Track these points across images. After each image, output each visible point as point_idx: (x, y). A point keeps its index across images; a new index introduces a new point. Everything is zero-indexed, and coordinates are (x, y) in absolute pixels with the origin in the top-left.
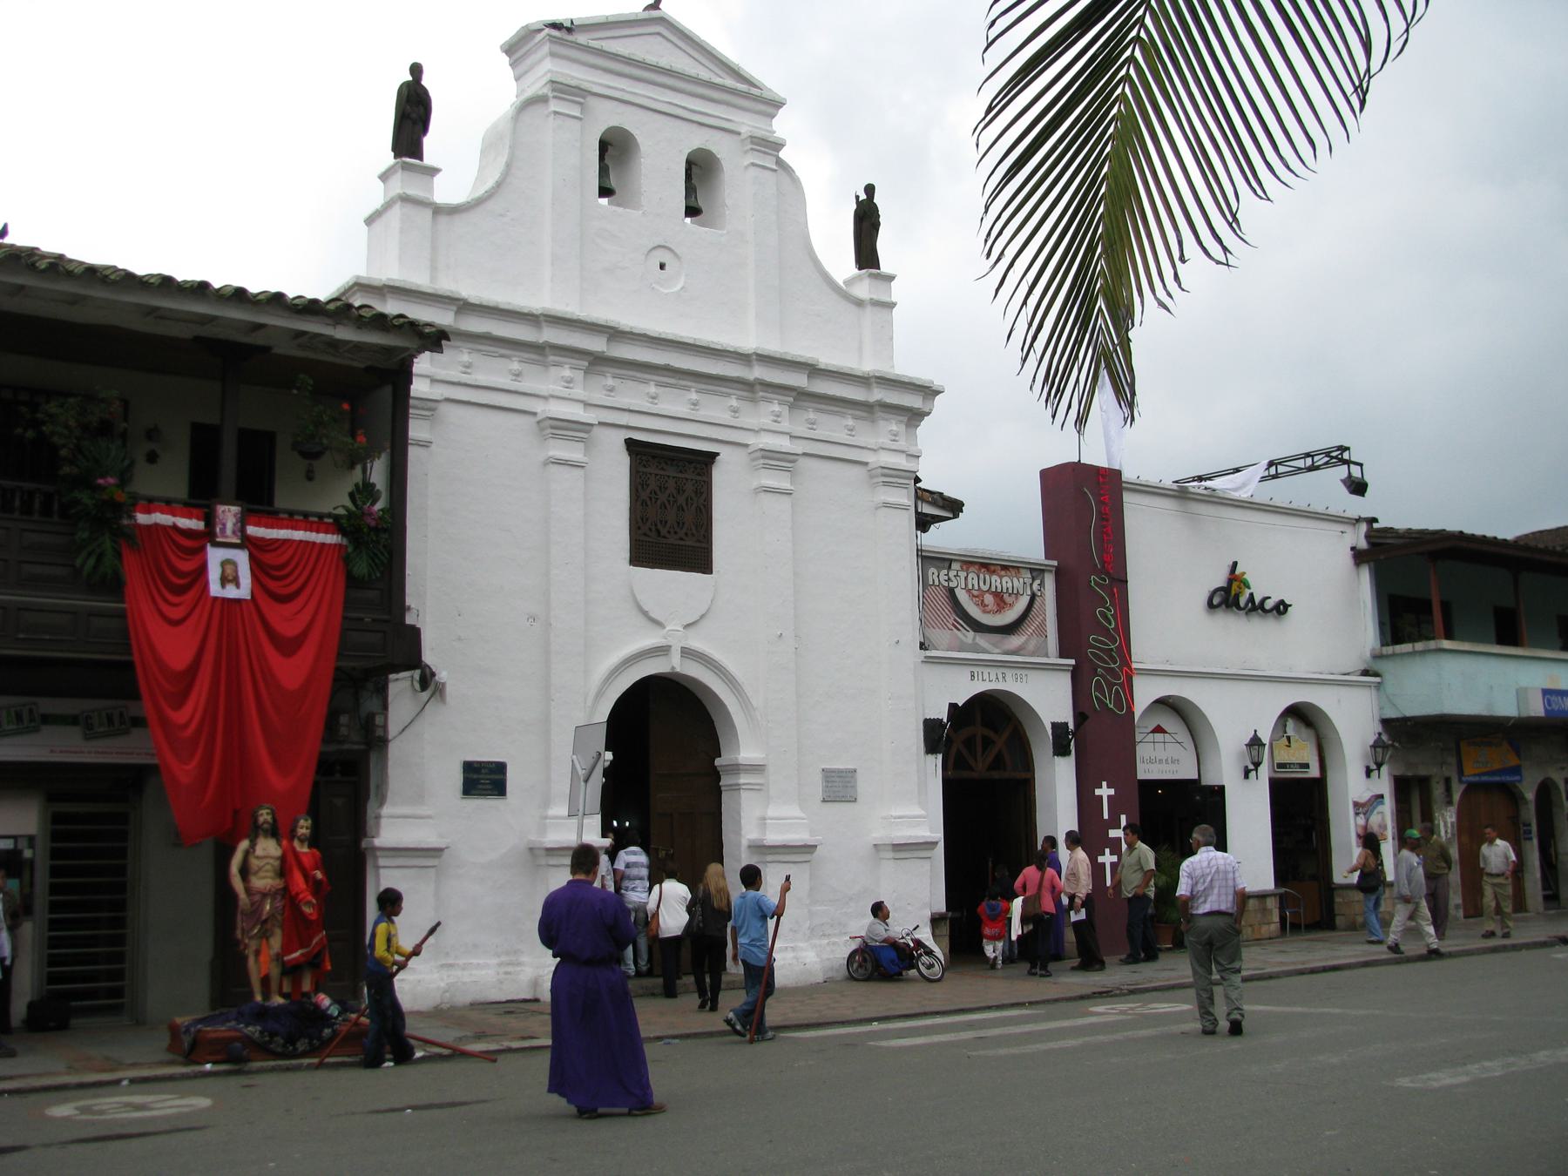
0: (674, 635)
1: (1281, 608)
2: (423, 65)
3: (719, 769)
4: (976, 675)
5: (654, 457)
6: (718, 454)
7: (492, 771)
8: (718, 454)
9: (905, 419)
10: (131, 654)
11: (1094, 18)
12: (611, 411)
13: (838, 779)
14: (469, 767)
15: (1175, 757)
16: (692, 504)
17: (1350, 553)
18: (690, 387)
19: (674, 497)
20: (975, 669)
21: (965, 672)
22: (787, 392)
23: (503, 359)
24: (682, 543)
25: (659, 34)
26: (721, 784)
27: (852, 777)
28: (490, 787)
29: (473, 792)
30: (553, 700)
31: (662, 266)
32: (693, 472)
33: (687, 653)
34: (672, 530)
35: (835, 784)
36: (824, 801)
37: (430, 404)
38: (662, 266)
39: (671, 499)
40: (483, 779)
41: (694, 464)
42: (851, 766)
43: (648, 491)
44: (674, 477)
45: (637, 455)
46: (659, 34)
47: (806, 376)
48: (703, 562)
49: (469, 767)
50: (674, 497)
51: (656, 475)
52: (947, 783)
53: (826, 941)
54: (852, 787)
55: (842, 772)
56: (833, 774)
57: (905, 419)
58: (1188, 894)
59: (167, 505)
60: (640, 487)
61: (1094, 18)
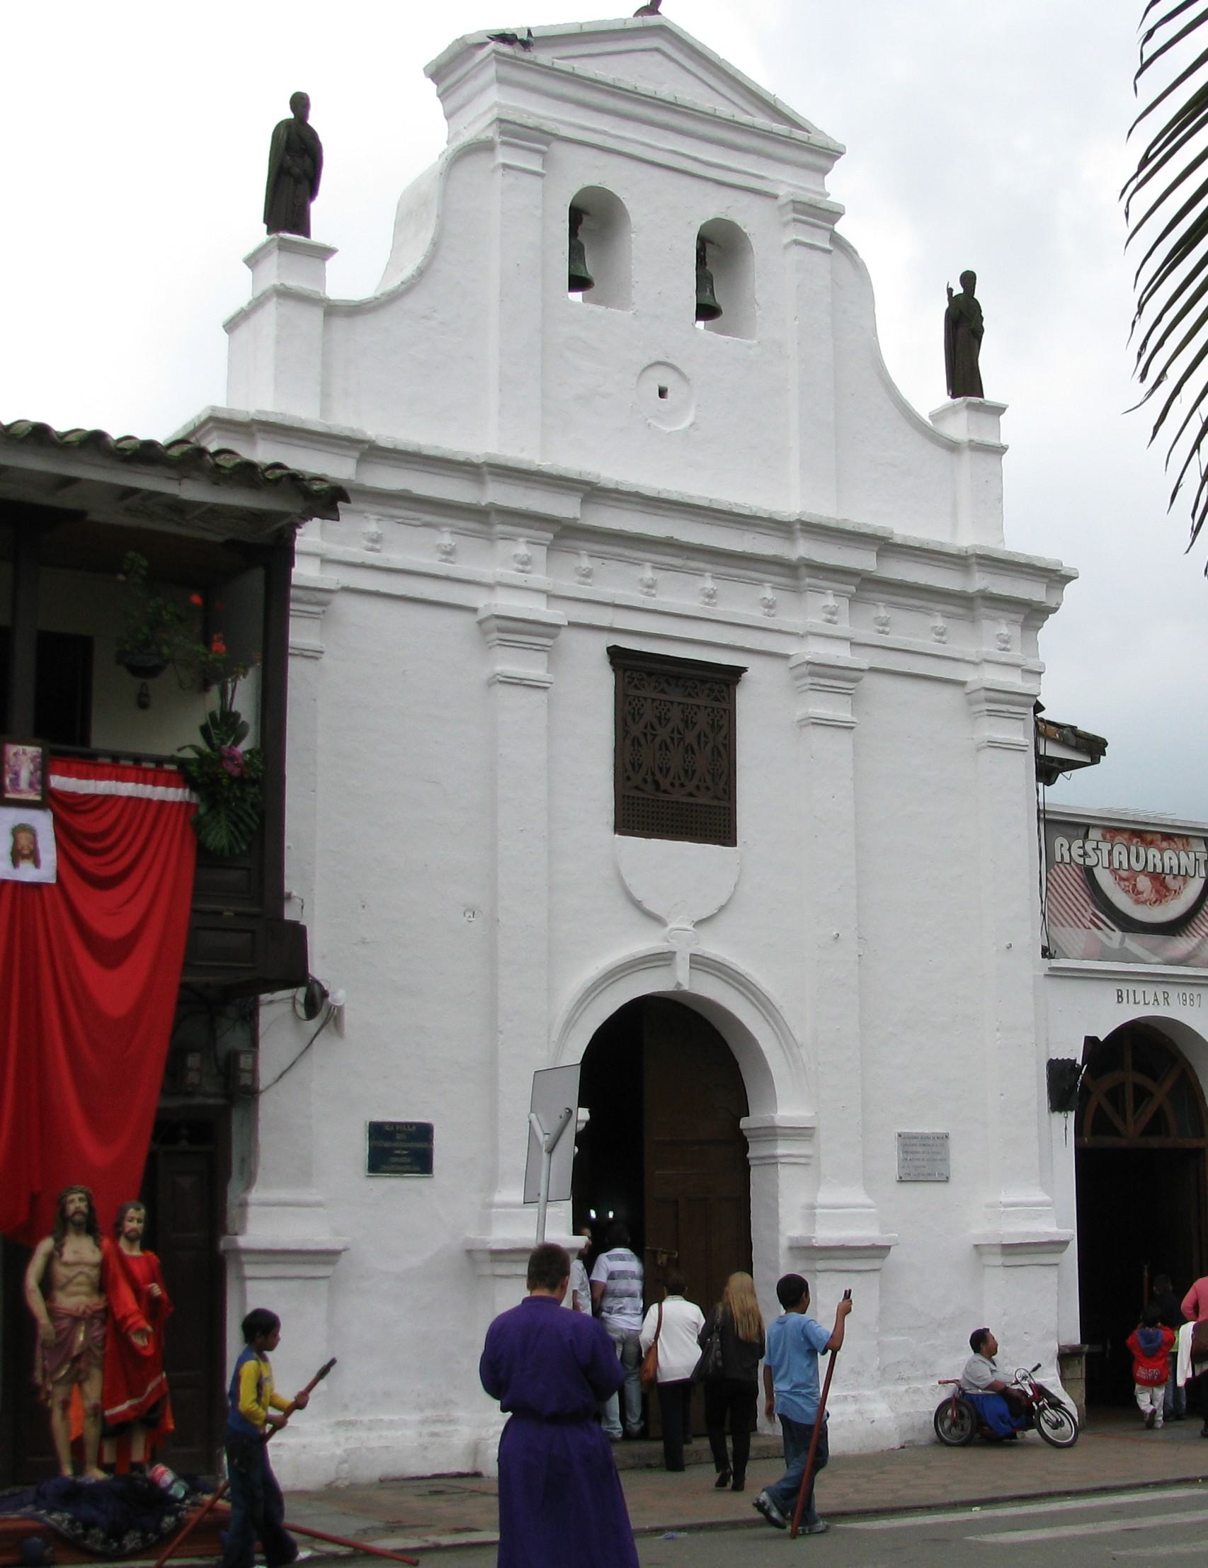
3: (745, 1133)
6: (744, 669)
8: (744, 669)
13: (920, 1149)
14: (378, 1132)
16: (706, 743)
19: (679, 733)
20: (1124, 987)
21: (1110, 990)
24: (691, 800)
25: (657, 50)
26: (748, 1155)
29: (384, 1167)
31: (662, 393)
33: (700, 963)
34: (677, 783)
35: (918, 1156)
36: (901, 1181)
37: (321, 596)
38: (662, 393)
39: (676, 735)
41: (708, 685)
42: (939, 1130)
43: (641, 725)
46: (657, 50)
49: (378, 1132)
50: (679, 733)
51: (654, 700)
54: (941, 1160)
56: (914, 1141)
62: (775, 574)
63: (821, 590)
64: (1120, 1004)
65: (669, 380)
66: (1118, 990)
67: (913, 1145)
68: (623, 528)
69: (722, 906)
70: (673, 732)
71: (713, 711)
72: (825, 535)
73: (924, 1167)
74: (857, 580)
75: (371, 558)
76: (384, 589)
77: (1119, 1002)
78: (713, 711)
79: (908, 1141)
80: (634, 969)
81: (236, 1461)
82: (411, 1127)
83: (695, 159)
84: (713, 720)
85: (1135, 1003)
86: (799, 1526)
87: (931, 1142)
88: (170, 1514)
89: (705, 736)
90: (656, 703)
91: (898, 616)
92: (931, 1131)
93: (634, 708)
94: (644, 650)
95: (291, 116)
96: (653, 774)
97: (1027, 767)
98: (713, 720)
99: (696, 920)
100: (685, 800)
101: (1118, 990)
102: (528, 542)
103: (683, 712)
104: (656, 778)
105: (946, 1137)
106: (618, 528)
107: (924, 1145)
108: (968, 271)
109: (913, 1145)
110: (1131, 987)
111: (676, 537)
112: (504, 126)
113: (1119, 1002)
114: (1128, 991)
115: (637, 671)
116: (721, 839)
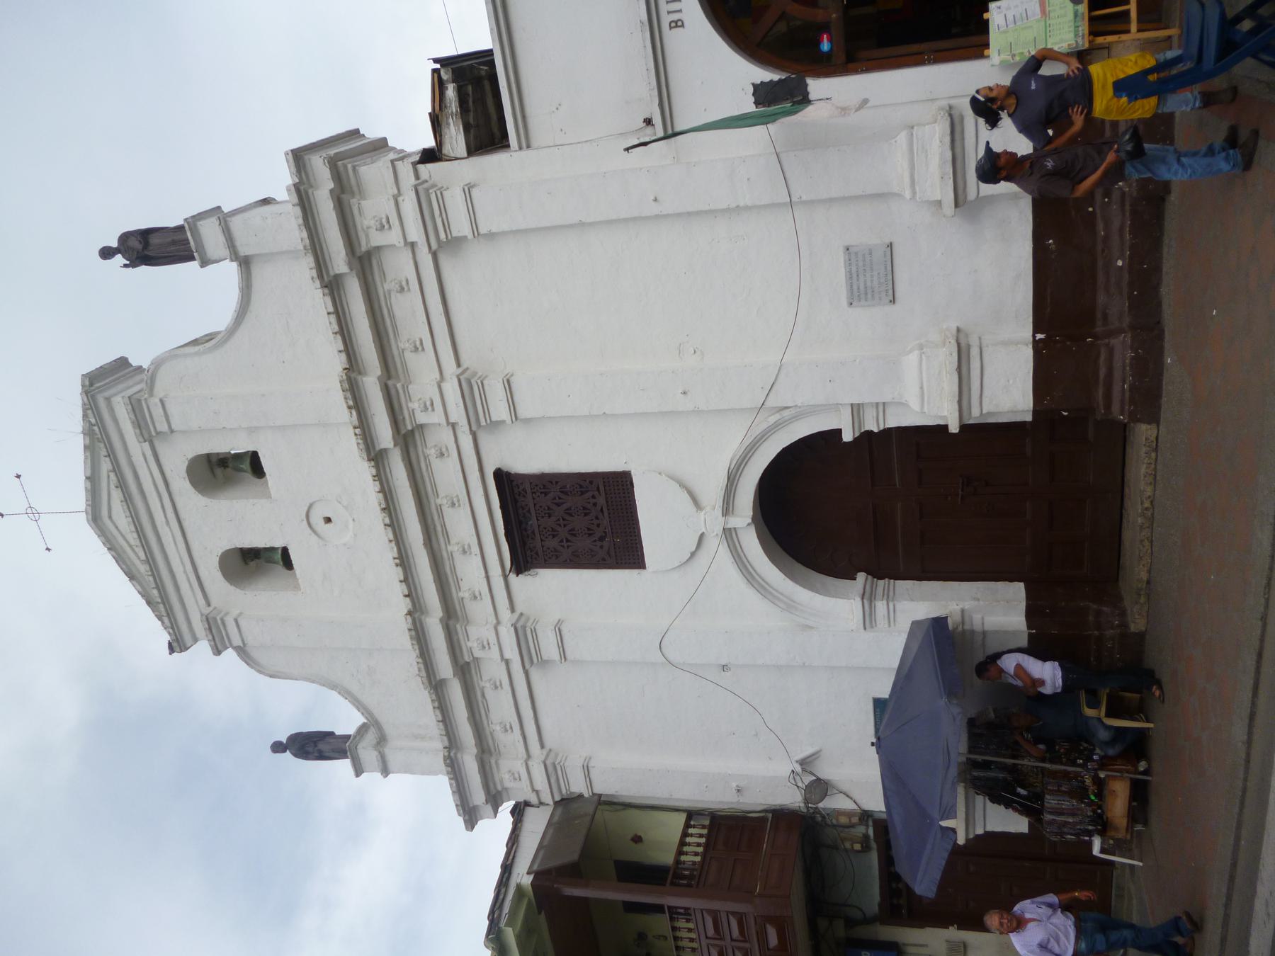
0: (713, 521)
1: (429, 59)
2: (271, 753)
3: (857, 434)
4: (675, 17)
9: (354, 201)
12: (495, 592)
13: (862, 278)
15: (799, 197)
16: (560, 498)
18: (436, 504)
20: (666, 19)
21: (673, 39)
22: (393, 392)
23: (486, 695)
24: (602, 488)
25: (110, 517)
26: (876, 430)
30: (804, 664)
31: (328, 520)
32: (524, 496)
33: (728, 506)
34: (592, 501)
35: (869, 284)
36: (893, 301)
37: (550, 769)
38: (328, 520)
41: (517, 497)
42: (841, 258)
43: (559, 529)
44: (538, 520)
45: (527, 562)
46: (110, 517)
47: (364, 379)
48: (620, 487)
51: (542, 540)
54: (871, 254)
55: (850, 272)
56: (855, 287)
57: (384, 506)
58: (1087, 45)
59: (692, 951)
62: (439, 544)
63: (411, 414)
64: (686, 24)
66: (671, 28)
67: (859, 289)
68: (432, 581)
69: (680, 486)
71: (535, 493)
72: (432, 664)
73: (879, 274)
74: (451, 623)
75: (476, 549)
76: (536, 738)
77: (683, 26)
78: (535, 493)
79: (856, 293)
80: (742, 555)
81: (1065, 414)
83: (163, 507)
84: (541, 493)
87: (854, 269)
89: (555, 499)
90: (543, 538)
91: (404, 334)
92: (843, 270)
94: (501, 516)
95: (285, 742)
96: (595, 541)
98: (541, 493)
99: (695, 509)
100: (606, 513)
101: (671, 28)
102: (468, 640)
103: (543, 517)
104: (597, 539)
106: (479, 776)
107: (858, 276)
108: (105, 247)
109: (859, 289)
111: (422, 542)
112: (220, 647)
113: (683, 26)
114: (669, 13)
115: (513, 491)
116: (637, 541)
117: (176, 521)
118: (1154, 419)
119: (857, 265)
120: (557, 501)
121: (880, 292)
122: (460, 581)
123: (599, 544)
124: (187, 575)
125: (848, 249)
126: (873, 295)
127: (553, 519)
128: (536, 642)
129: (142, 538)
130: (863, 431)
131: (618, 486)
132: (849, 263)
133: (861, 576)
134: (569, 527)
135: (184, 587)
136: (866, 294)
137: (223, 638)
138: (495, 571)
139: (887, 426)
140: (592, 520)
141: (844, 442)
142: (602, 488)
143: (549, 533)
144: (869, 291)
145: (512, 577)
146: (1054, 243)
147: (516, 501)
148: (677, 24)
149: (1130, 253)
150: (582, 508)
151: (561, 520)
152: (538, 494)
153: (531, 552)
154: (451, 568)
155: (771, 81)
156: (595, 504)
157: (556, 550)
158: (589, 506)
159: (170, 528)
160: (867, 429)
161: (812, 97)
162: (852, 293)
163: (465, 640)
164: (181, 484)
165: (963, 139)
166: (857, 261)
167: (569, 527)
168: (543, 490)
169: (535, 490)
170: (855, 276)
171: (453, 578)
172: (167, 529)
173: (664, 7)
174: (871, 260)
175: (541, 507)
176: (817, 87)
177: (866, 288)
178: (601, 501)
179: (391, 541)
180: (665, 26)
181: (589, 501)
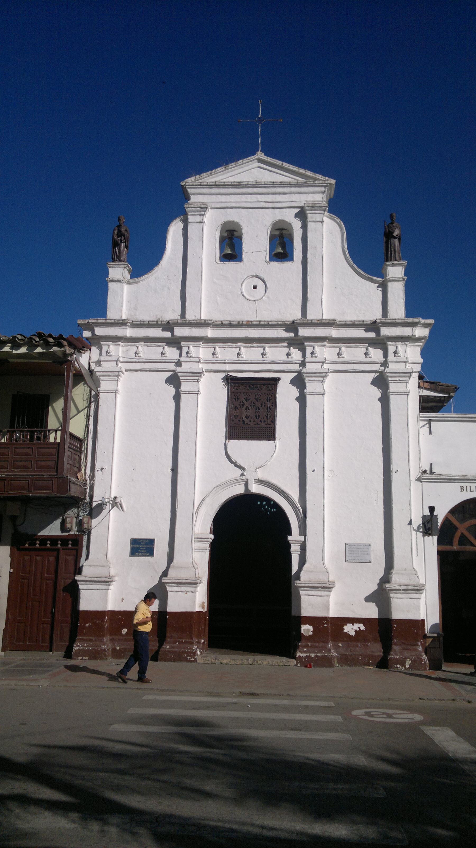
4: (465, 489)
5: (242, 385)
6: (279, 379)
7: (146, 544)
8: (279, 379)
10: (45, 428)
11: (41, 491)
14: (135, 542)
16: (265, 406)
17: (416, 481)
19: (254, 403)
21: (457, 486)
24: (269, 426)
27: (368, 548)
28: (146, 551)
29: (137, 554)
31: (255, 287)
34: (252, 420)
38: (255, 287)
39: (252, 404)
40: (142, 548)
41: (245, 385)
42: (365, 541)
49: (135, 542)
50: (254, 403)
52: (440, 553)
53: (10, 611)
54: (367, 554)
56: (354, 547)
60: (234, 400)
61: (41, 491)
64: (462, 492)
65: (260, 284)
70: (251, 403)
78: (268, 394)
80: (238, 484)
82: (147, 540)
84: (268, 398)
85: (471, 491)
86: (443, 400)
87: (361, 547)
88: (80, 644)
89: (264, 403)
93: (236, 397)
97: (205, 597)
102: (244, 348)
103: (255, 396)
105: (370, 545)
110: (468, 485)
113: (461, 491)
114: (467, 487)
117: (226, 206)
118: (89, 659)
119: (363, 548)
120: (263, 404)
121: (351, 556)
122: (224, 348)
123: (241, 420)
124: (228, 202)
125: (370, 545)
126: (350, 554)
127: (244, 401)
128: (108, 380)
129: (251, 186)
130: (291, 544)
131: (270, 434)
132: (364, 545)
133: (212, 536)
134: (250, 407)
135: (222, 198)
136: (351, 551)
137: (194, 212)
138: (229, 367)
139: (292, 555)
140: (253, 419)
141: (287, 536)
142: (269, 426)
143: (247, 397)
144: (353, 552)
145: (223, 375)
146: (78, 624)
147: (264, 385)
148: (462, 489)
149: (90, 650)
150: (259, 415)
151: (254, 404)
152: (267, 396)
153: (238, 387)
154: (232, 346)
155: (438, 522)
156: (261, 421)
157: (238, 399)
158: (260, 418)
159: (256, 202)
160: (292, 546)
161: (426, 537)
162: (352, 545)
163: (193, 344)
164: (279, 215)
165: (414, 593)
166: (366, 546)
167: (250, 407)
168: (269, 398)
169: (269, 395)
170: (359, 547)
171: (226, 346)
172: (255, 200)
173: (473, 486)
174: (365, 554)
175: (261, 396)
176: (432, 541)
177: (354, 551)
178: (263, 424)
179: (179, 315)
180: (462, 484)
181: (263, 419)
